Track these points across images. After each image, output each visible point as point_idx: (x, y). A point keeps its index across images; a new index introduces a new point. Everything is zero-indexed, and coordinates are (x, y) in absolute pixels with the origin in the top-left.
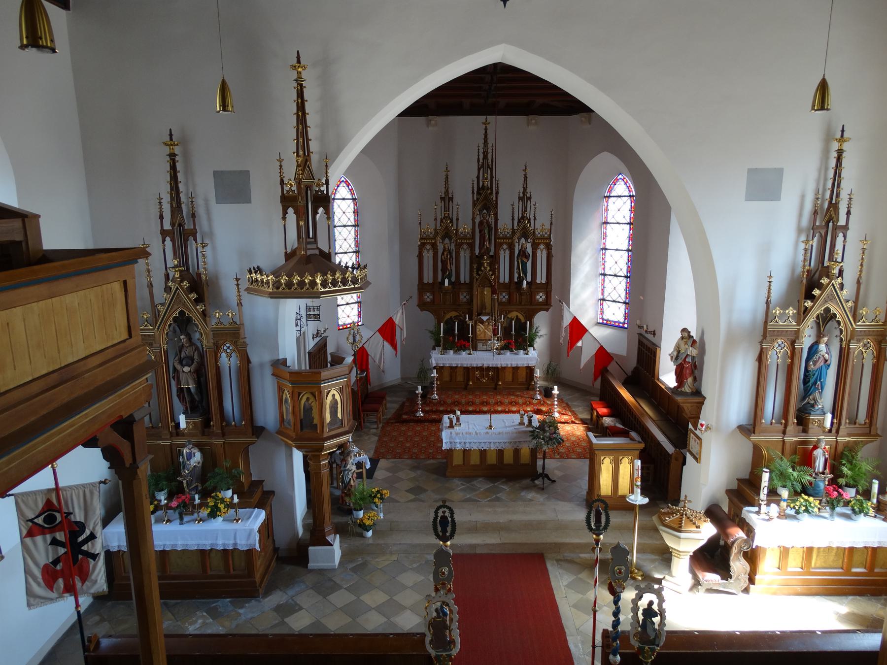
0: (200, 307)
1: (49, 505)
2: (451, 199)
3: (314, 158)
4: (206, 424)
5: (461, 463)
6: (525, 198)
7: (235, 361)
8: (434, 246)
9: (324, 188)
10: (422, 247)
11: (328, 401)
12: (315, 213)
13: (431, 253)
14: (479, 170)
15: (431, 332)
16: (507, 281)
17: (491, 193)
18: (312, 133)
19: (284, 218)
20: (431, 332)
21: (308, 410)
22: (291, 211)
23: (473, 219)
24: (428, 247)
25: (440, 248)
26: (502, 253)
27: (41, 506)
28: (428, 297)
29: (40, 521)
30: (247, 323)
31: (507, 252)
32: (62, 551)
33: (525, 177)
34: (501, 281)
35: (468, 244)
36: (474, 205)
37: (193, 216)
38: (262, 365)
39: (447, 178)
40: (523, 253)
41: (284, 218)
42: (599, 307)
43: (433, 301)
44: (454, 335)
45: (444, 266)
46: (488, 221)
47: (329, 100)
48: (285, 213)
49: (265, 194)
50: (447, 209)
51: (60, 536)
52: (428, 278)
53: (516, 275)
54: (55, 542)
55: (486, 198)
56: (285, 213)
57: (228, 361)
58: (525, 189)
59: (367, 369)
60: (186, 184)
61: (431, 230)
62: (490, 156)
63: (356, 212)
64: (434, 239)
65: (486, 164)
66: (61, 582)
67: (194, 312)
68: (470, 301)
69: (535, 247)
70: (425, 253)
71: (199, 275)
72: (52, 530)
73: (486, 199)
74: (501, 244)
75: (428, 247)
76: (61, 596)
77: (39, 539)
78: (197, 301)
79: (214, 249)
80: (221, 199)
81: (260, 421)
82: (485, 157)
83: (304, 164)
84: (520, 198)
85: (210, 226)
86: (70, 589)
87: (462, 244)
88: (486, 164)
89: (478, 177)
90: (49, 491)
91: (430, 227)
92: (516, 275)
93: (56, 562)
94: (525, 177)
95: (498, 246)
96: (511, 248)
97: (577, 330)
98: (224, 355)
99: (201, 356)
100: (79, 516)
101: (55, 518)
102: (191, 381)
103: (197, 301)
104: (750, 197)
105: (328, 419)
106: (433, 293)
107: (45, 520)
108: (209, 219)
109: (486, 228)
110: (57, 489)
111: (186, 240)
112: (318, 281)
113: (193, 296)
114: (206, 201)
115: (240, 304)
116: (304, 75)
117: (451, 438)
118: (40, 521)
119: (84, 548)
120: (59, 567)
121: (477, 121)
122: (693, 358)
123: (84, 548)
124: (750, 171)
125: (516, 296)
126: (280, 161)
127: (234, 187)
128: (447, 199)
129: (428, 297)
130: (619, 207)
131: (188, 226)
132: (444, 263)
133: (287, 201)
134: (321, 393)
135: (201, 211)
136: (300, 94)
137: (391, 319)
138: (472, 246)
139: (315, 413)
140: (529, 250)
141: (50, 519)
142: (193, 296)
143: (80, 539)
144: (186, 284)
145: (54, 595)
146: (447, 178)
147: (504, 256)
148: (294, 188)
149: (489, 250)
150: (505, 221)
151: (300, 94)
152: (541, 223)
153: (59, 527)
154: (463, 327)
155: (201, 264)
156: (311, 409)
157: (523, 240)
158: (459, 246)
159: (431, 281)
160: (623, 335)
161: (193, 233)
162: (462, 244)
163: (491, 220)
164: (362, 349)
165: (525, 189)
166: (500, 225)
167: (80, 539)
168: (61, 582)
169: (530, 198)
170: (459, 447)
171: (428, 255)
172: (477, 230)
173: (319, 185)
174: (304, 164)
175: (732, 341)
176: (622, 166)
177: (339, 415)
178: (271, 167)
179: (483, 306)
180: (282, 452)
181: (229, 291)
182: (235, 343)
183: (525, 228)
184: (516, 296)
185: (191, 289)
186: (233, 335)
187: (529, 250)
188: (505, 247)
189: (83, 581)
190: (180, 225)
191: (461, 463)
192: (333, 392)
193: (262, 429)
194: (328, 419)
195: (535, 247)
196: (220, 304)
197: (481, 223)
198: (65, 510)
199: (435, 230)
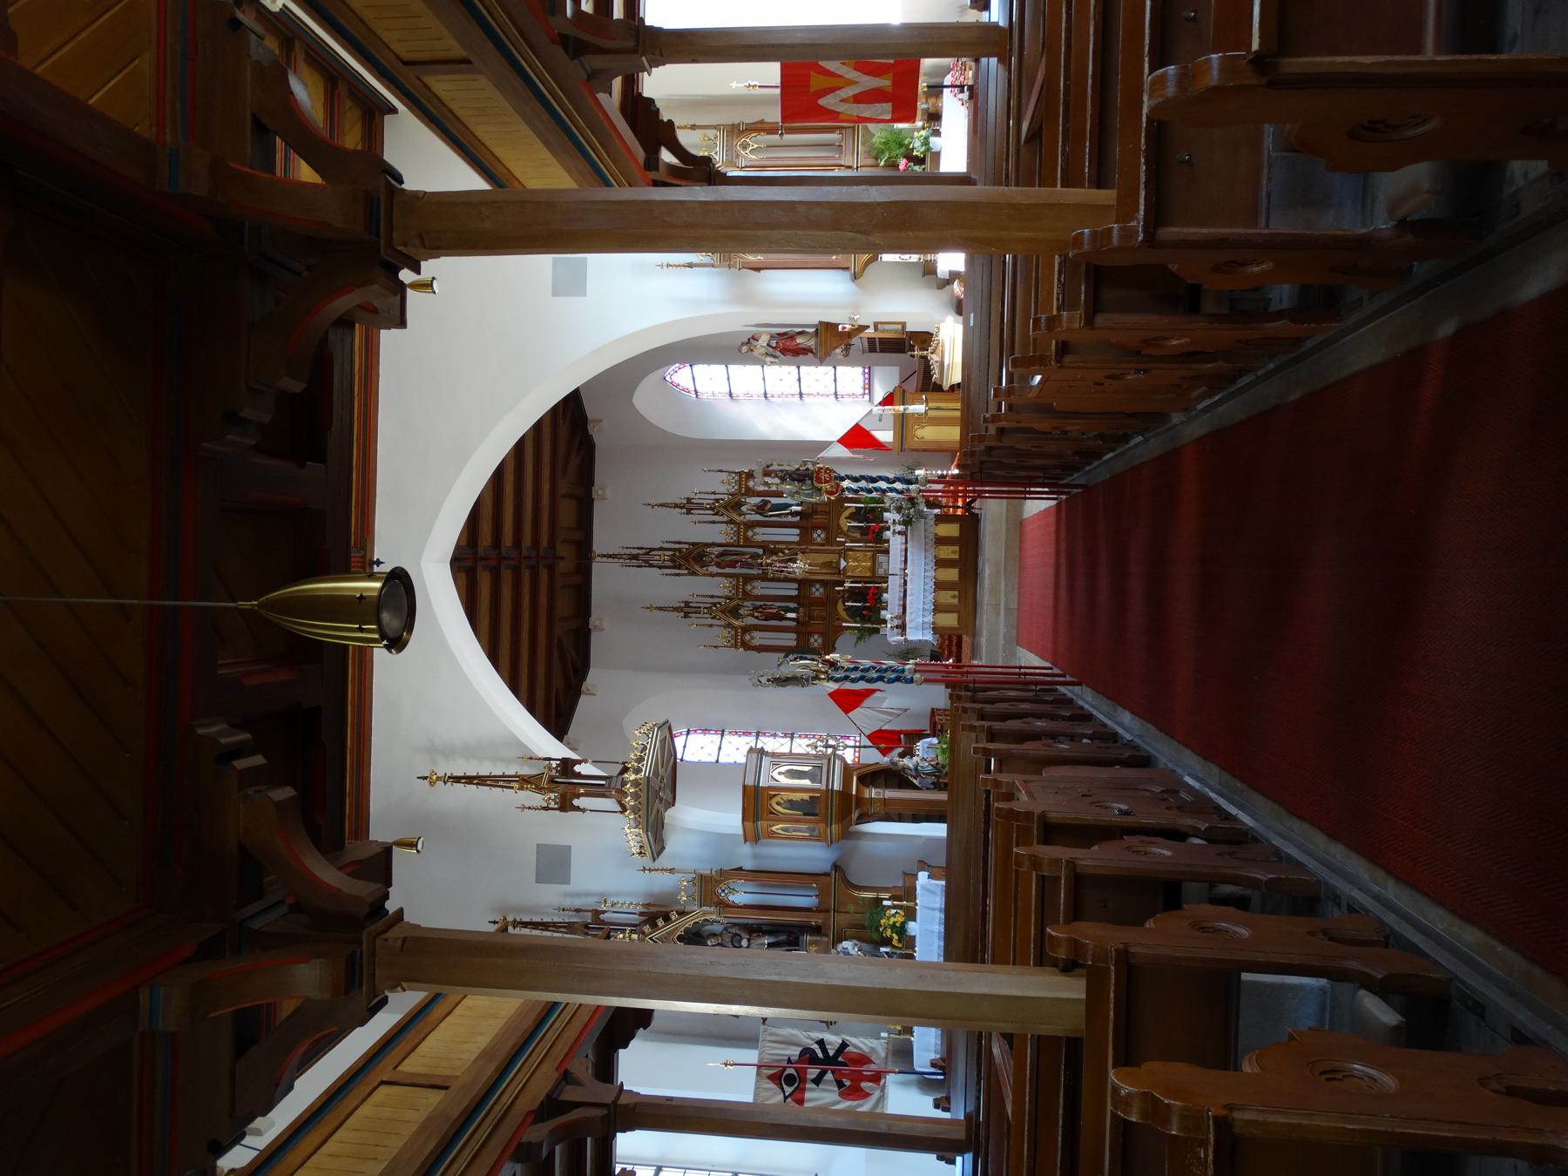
0: (674, 916)
1: (776, 1078)
2: (687, 604)
3: (526, 770)
4: (817, 930)
5: (955, 616)
6: (688, 506)
7: (739, 884)
8: (747, 629)
9: (554, 764)
10: (747, 646)
11: (785, 781)
12: (579, 775)
13: (756, 634)
14: (651, 566)
15: (859, 639)
16: (797, 531)
17: (680, 550)
18: (498, 771)
19: (584, 810)
20: (859, 639)
21: (792, 804)
22: (576, 802)
23: (712, 575)
24: (747, 637)
25: (750, 621)
26: (759, 538)
27: (773, 1086)
28: (816, 640)
29: (789, 1090)
30: (691, 866)
31: (758, 530)
32: (829, 1076)
33: (662, 505)
34: (797, 539)
35: (745, 584)
36: (693, 573)
37: (578, 911)
38: (756, 857)
39: (661, 609)
40: (760, 509)
41: (584, 810)
42: (847, 399)
43: (821, 634)
44: (864, 608)
45: (770, 615)
46: (718, 556)
47: (471, 751)
48: (578, 809)
49: (558, 828)
50: (697, 610)
51: (813, 1072)
52: (789, 640)
53: (790, 518)
54: (817, 1081)
55: (686, 557)
56: (578, 809)
57: (741, 895)
58: (676, 506)
59: (898, 733)
60: (548, 914)
61: (725, 632)
62: (635, 552)
63: (706, 731)
64: (735, 628)
65: (641, 558)
66: (865, 1085)
67: (681, 925)
68: (823, 583)
69: (751, 493)
70: (756, 642)
71: (641, 914)
72: (803, 1080)
73: (689, 558)
74: (746, 538)
75: (747, 637)
76: (883, 1089)
77: (808, 1095)
78: (667, 919)
79: (618, 894)
80: (566, 880)
81: (825, 867)
82: (635, 557)
83: (525, 781)
84: (688, 512)
85: (593, 895)
86: (877, 1078)
87: (744, 592)
88: (641, 558)
89: (660, 567)
90: (758, 1074)
91: (720, 634)
92: (790, 518)
93: (840, 1084)
94: (662, 505)
95: (749, 543)
96: (752, 525)
97: (857, 437)
98: (731, 898)
99: (735, 925)
100: (795, 1052)
101: (790, 1075)
102: (760, 941)
103: (667, 919)
104: (582, 291)
105: (806, 782)
106: (811, 634)
107: (790, 1085)
108: (587, 895)
109: (726, 558)
110: (759, 1067)
111: (603, 922)
112: (633, 777)
113: (660, 922)
114: (567, 895)
115: (672, 871)
116: (441, 774)
117: (916, 628)
118: (789, 1090)
119: (831, 1053)
120: (848, 1083)
121: (597, 567)
122: (772, 337)
123: (831, 1053)
124: (555, 294)
125: (819, 518)
126: (524, 808)
127: (554, 863)
128: (687, 609)
129: (816, 640)
130: (707, 379)
131: (588, 918)
132: (769, 617)
133: (565, 805)
134: (770, 788)
135: (577, 903)
136: (457, 779)
137: (831, 695)
138: (748, 579)
139: (797, 796)
140: (756, 500)
141: (790, 1080)
142: (660, 922)
143: (820, 1055)
144: (647, 929)
145: (877, 1094)
146: (661, 609)
147: (762, 535)
148: (552, 796)
149: (755, 556)
150: (716, 533)
151: (457, 779)
152: (720, 485)
153: (802, 1075)
154: (854, 594)
155: (631, 909)
156: (791, 801)
157: (744, 508)
158: (747, 596)
159: (794, 636)
160: (878, 372)
161: (597, 913)
162: (744, 592)
163: (716, 550)
164: (870, 737)
165: (676, 506)
166: (721, 539)
167: (820, 1055)
168: (865, 1085)
169: (689, 500)
170: (930, 618)
171: (758, 638)
172: (728, 570)
173: (550, 768)
174: (525, 781)
175: (746, 298)
176: (657, 374)
177: (806, 769)
178: (530, 821)
179: (828, 565)
180: (865, 844)
181: (661, 883)
182: (718, 882)
183: (725, 507)
184: (819, 518)
185: (654, 926)
186: (708, 886)
187: (756, 500)
188: (750, 533)
189: (870, 1061)
190: (586, 926)
191: (955, 616)
192: (775, 774)
193: (836, 867)
194: (806, 782)
195: (751, 493)
196: (672, 897)
197: (719, 565)
198: (785, 1064)
199: (725, 627)
